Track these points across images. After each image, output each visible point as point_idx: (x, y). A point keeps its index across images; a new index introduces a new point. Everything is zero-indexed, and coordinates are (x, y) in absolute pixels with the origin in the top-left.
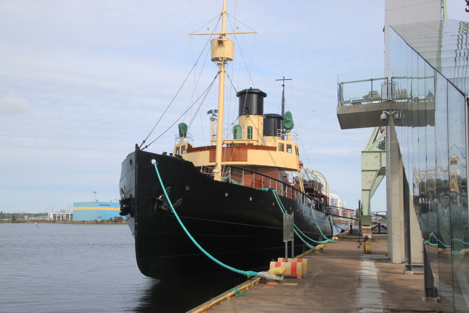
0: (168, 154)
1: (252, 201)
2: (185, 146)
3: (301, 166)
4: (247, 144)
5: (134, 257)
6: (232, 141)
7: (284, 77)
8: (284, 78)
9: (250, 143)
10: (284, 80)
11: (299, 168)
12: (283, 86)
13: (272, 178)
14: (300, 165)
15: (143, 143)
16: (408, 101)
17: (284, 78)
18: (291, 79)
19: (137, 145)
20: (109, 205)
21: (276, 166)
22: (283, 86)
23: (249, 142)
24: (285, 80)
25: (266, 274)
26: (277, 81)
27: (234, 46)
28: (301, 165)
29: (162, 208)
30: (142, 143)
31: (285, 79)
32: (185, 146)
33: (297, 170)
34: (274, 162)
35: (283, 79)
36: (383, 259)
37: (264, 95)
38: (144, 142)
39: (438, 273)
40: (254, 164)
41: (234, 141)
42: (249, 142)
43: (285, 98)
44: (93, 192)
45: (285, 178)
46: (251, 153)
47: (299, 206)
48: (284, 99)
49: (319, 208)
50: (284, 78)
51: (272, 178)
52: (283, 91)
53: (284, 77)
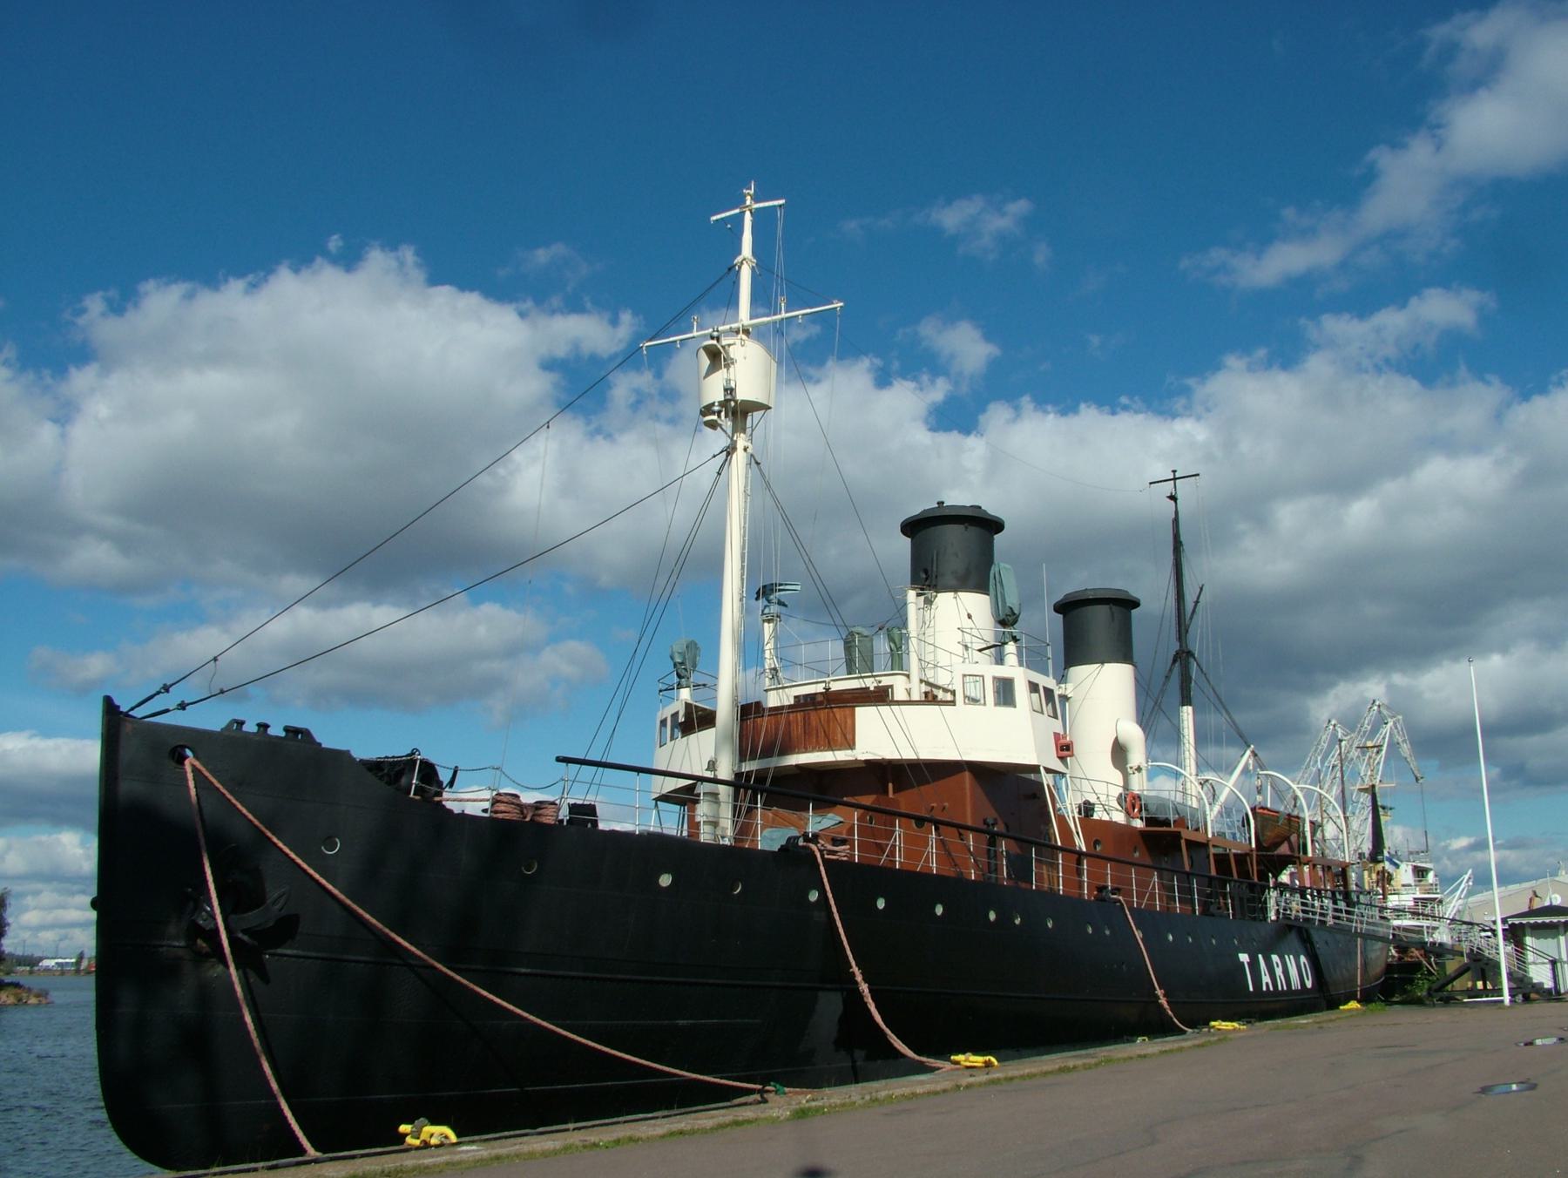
2: (677, 713)
3: (1066, 753)
4: (875, 687)
7: (1174, 472)
8: (1177, 474)
10: (1175, 479)
12: (1173, 498)
14: (1062, 750)
17: (1174, 475)
18: (1198, 475)
20: (559, 759)
22: (1173, 498)
23: (880, 682)
24: (1178, 481)
26: (1152, 485)
27: (704, 685)
31: (1177, 476)
32: (677, 713)
33: (1039, 766)
35: (1172, 477)
36: (910, 701)
37: (993, 526)
38: (166, 689)
39: (874, 653)
42: (880, 682)
43: (1182, 538)
44: (789, 606)
46: (865, 716)
48: (1181, 542)
50: (1174, 475)
53: (1174, 472)
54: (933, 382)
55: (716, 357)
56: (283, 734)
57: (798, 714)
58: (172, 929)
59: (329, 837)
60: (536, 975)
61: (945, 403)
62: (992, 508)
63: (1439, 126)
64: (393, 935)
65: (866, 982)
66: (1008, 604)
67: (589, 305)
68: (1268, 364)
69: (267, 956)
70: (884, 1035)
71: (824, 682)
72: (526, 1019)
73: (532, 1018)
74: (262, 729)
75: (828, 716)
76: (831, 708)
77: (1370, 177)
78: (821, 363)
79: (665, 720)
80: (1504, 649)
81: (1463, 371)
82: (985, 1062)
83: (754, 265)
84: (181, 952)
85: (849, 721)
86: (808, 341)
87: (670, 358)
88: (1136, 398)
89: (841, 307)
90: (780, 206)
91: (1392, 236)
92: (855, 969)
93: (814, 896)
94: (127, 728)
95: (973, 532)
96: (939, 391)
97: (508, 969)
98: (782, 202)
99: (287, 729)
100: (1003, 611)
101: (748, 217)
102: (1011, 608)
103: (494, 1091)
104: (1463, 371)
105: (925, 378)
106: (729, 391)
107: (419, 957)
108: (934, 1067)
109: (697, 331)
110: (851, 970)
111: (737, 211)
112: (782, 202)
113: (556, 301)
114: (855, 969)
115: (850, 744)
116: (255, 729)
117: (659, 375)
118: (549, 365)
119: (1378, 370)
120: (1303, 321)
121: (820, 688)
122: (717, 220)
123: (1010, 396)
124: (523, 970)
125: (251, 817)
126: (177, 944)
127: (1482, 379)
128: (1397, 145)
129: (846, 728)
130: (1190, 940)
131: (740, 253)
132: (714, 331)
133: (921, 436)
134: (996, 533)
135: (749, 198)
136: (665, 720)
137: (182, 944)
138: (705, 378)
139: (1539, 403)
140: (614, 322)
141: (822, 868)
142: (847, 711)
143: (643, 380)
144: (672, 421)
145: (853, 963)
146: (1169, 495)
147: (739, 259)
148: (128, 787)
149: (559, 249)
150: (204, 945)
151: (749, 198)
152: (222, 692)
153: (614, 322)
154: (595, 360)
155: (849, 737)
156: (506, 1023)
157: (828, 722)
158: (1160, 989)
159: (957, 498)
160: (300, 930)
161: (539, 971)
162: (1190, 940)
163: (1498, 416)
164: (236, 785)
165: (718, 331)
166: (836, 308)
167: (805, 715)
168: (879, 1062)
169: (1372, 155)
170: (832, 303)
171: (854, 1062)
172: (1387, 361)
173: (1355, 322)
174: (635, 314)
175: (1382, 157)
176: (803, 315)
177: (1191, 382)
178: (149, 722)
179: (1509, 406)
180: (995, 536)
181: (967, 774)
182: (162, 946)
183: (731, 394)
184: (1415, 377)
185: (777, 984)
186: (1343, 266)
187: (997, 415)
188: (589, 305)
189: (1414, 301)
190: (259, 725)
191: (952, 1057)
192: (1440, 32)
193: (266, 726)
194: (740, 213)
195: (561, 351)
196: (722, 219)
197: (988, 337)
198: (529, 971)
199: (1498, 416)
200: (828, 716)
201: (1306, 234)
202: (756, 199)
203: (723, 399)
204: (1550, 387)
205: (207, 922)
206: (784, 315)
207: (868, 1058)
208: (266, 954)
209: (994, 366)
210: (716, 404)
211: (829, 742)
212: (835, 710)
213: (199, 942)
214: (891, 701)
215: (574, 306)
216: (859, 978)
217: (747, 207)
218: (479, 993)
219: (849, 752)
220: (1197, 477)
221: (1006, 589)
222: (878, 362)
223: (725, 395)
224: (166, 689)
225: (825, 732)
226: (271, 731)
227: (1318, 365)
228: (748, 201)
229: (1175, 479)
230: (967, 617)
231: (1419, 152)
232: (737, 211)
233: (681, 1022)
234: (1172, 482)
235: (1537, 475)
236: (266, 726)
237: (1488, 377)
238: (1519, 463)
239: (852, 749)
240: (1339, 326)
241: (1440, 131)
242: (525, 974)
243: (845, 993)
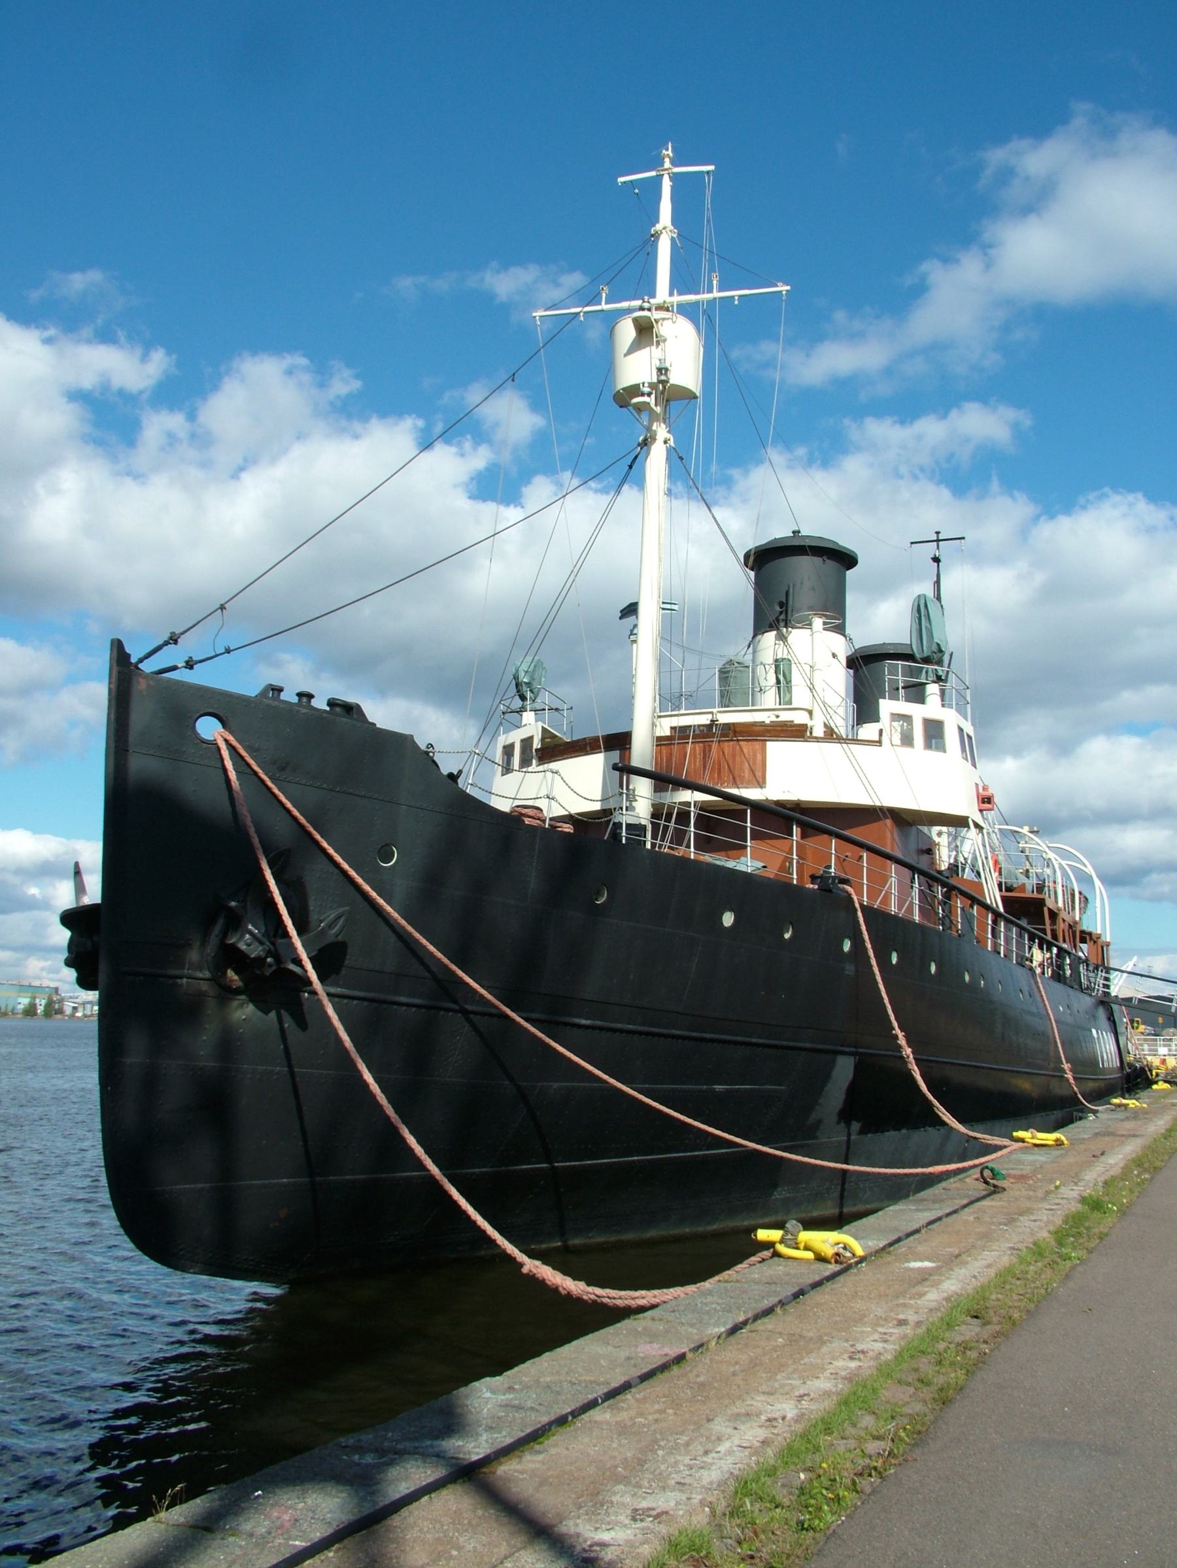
0: (289, 696)
1: (850, 951)
2: (531, 738)
3: (987, 806)
5: (100, 1167)
6: (710, 717)
7: (938, 533)
8: (940, 535)
9: (779, 719)
10: (938, 541)
11: (979, 813)
12: (936, 560)
13: (870, 849)
14: (983, 802)
15: (166, 643)
16: (648, 1431)
17: (938, 537)
18: (963, 538)
19: (118, 648)
21: (844, 745)
22: (936, 560)
23: (777, 717)
24: (941, 543)
25: (548, 1469)
28: (986, 801)
29: (242, 946)
30: (161, 643)
31: (940, 538)
32: (531, 738)
33: (968, 817)
34: (867, 785)
35: (935, 539)
37: (847, 560)
38: (174, 639)
40: (796, 799)
41: (718, 714)
45: (925, 857)
46: (777, 752)
47: (1102, 1058)
49: (906, 1265)
50: (938, 537)
51: (870, 849)
52: (935, 579)
53: (938, 533)
54: (475, 449)
55: (645, 332)
56: (295, 700)
57: (697, 745)
58: (194, 955)
59: (387, 845)
60: (601, 1029)
61: (487, 469)
62: (845, 542)
63: (990, 246)
64: (454, 967)
65: (909, 1047)
66: (936, 640)
67: (122, 339)
68: (809, 462)
69: (306, 994)
70: (930, 1105)
71: (712, 713)
72: (605, 1082)
73: (612, 1081)
74: (305, 700)
75: (734, 749)
76: (738, 740)
77: (920, 289)
78: (365, 419)
79: (512, 746)
80: (1017, 752)
81: (995, 485)
82: (1057, 1140)
83: (675, 236)
84: (205, 986)
85: (759, 757)
86: (350, 396)
87: (205, 399)
88: (679, 484)
89: (787, 291)
90: (708, 172)
91: (935, 349)
92: (897, 1031)
93: (847, 946)
94: (140, 686)
95: (831, 565)
96: (480, 459)
97: (567, 1020)
98: (711, 168)
99: (332, 703)
100: (929, 647)
101: (667, 185)
102: (938, 645)
103: (524, 1167)
104: (995, 485)
105: (468, 445)
106: (662, 371)
107: (488, 1001)
108: (996, 1145)
109: (606, 303)
110: (894, 1032)
111: (653, 174)
112: (711, 168)
113: (87, 332)
114: (897, 1031)
115: (761, 783)
116: (295, 700)
117: (192, 417)
118: (77, 396)
119: (915, 478)
120: (846, 422)
121: (705, 720)
122: (625, 182)
123: (549, 470)
124: (583, 1022)
125: (296, 813)
126: (200, 975)
127: (1011, 496)
128: (948, 260)
129: (755, 763)
130: (1061, 1009)
131: (658, 221)
132: (644, 302)
133: (462, 502)
134: (848, 569)
135: (667, 160)
136: (512, 746)
137: (207, 974)
138: (625, 355)
139: (1064, 524)
140: (145, 358)
141: (860, 914)
142: (757, 745)
143: (175, 421)
144: (205, 465)
145: (895, 1024)
146: (932, 556)
147: (658, 227)
148: (140, 764)
149: (95, 276)
150: (236, 977)
151: (667, 160)
152: (228, 651)
153: (145, 358)
154: (124, 396)
155: (758, 774)
156: (556, 1085)
157: (734, 756)
158: (1067, 1063)
159: (814, 528)
160: (347, 962)
161: (598, 1023)
162: (1061, 1009)
163: (1024, 533)
164: (281, 768)
165: (649, 302)
166: (781, 291)
167: (704, 747)
168: (869, 1135)
169: (925, 267)
170: (777, 286)
171: (849, 1135)
172: (922, 469)
173: (897, 426)
174: (169, 354)
175: (934, 271)
176: (740, 296)
177: (735, 473)
178: (170, 680)
179: (1038, 517)
180: (848, 572)
181: (889, 822)
182: (181, 978)
183: (666, 374)
184: (947, 486)
185: (808, 1045)
186: (888, 372)
187: (539, 490)
188: (122, 339)
189: (954, 413)
190: (300, 695)
191: (1015, 1134)
192: (996, 156)
193: (310, 696)
194: (657, 175)
195: (88, 382)
196: (631, 181)
197: (537, 405)
198: (588, 1022)
199: (1024, 533)
200: (734, 749)
201: (856, 337)
202: (674, 163)
203: (655, 380)
204: (1077, 507)
205: (252, 947)
206: (716, 294)
207: (862, 1132)
208: (305, 992)
209: (540, 442)
210: (646, 385)
211: (734, 778)
212: (742, 743)
213: (230, 973)
214: (809, 737)
215: (106, 337)
216: (902, 1041)
217: (666, 170)
218: (555, 1049)
219: (759, 790)
220: (963, 541)
221: (933, 623)
222: (421, 423)
223: (658, 376)
224: (174, 639)
225: (729, 766)
226: (315, 703)
227: (855, 466)
228: (667, 164)
229: (938, 541)
230: (831, 657)
231: (970, 268)
232: (653, 174)
233: (718, 1087)
234: (935, 543)
235: (1053, 592)
236: (310, 696)
237: (1016, 493)
238: (1040, 578)
239: (761, 788)
240: (881, 430)
241: (989, 251)
242: (586, 1027)
243: (857, 1057)
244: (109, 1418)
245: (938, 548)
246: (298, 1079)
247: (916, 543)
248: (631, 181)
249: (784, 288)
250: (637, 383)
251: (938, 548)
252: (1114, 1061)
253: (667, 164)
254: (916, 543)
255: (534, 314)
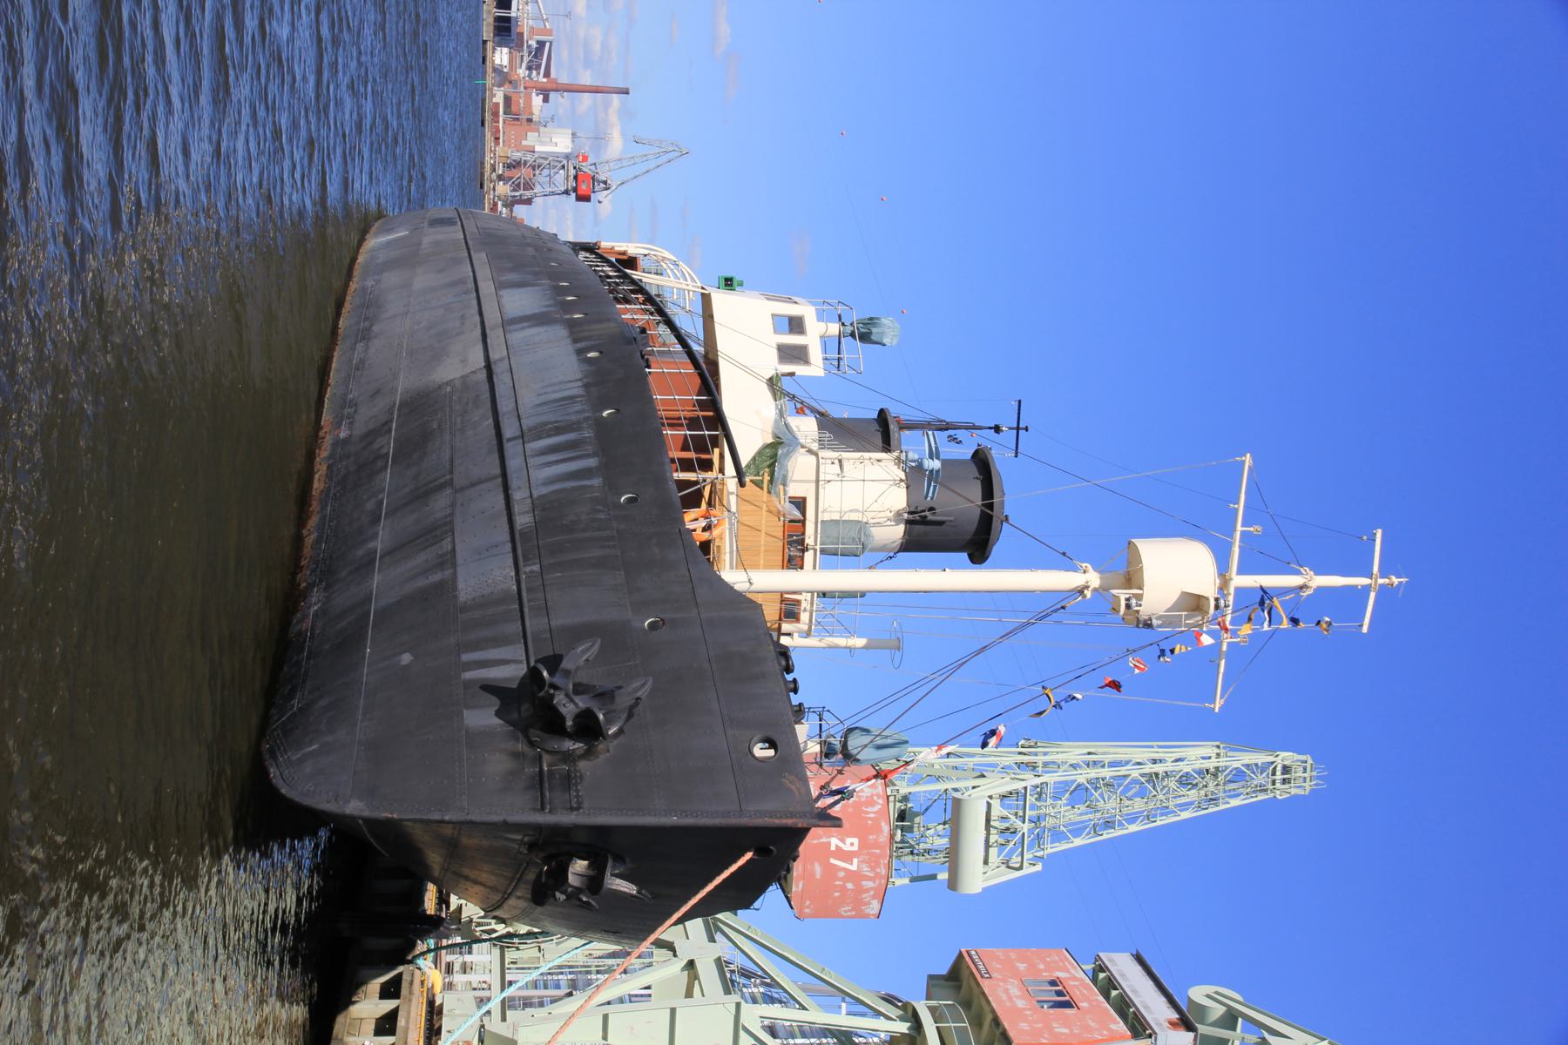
7: (1026, 429)
17: (1022, 429)
24: (1015, 431)
35: (1021, 426)
50: (1022, 429)
90: (1361, 626)
98: (1365, 629)
112: (1365, 629)
121: (809, 541)
134: (968, 555)
166: (1214, 703)
228: (1381, 581)
234: (1016, 426)
244: (218, 110)
245: (1010, 428)
246: (522, 641)
247: (1019, 406)
248: (1375, 540)
249: (1218, 704)
250: (1145, 588)
251: (1010, 428)
252: (357, 170)
253: (1381, 581)
254: (1019, 406)
255: (1248, 455)
